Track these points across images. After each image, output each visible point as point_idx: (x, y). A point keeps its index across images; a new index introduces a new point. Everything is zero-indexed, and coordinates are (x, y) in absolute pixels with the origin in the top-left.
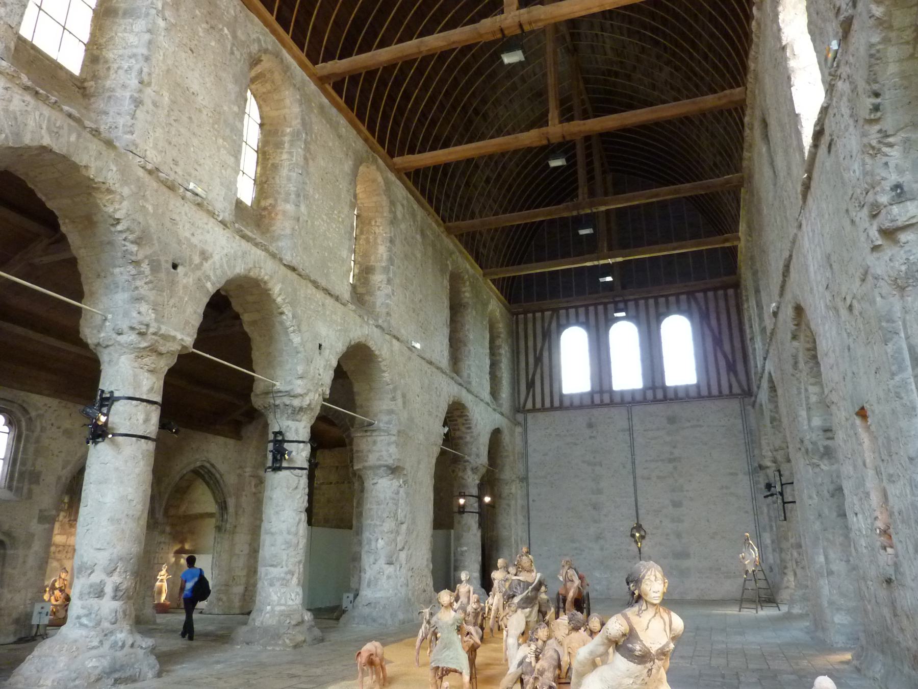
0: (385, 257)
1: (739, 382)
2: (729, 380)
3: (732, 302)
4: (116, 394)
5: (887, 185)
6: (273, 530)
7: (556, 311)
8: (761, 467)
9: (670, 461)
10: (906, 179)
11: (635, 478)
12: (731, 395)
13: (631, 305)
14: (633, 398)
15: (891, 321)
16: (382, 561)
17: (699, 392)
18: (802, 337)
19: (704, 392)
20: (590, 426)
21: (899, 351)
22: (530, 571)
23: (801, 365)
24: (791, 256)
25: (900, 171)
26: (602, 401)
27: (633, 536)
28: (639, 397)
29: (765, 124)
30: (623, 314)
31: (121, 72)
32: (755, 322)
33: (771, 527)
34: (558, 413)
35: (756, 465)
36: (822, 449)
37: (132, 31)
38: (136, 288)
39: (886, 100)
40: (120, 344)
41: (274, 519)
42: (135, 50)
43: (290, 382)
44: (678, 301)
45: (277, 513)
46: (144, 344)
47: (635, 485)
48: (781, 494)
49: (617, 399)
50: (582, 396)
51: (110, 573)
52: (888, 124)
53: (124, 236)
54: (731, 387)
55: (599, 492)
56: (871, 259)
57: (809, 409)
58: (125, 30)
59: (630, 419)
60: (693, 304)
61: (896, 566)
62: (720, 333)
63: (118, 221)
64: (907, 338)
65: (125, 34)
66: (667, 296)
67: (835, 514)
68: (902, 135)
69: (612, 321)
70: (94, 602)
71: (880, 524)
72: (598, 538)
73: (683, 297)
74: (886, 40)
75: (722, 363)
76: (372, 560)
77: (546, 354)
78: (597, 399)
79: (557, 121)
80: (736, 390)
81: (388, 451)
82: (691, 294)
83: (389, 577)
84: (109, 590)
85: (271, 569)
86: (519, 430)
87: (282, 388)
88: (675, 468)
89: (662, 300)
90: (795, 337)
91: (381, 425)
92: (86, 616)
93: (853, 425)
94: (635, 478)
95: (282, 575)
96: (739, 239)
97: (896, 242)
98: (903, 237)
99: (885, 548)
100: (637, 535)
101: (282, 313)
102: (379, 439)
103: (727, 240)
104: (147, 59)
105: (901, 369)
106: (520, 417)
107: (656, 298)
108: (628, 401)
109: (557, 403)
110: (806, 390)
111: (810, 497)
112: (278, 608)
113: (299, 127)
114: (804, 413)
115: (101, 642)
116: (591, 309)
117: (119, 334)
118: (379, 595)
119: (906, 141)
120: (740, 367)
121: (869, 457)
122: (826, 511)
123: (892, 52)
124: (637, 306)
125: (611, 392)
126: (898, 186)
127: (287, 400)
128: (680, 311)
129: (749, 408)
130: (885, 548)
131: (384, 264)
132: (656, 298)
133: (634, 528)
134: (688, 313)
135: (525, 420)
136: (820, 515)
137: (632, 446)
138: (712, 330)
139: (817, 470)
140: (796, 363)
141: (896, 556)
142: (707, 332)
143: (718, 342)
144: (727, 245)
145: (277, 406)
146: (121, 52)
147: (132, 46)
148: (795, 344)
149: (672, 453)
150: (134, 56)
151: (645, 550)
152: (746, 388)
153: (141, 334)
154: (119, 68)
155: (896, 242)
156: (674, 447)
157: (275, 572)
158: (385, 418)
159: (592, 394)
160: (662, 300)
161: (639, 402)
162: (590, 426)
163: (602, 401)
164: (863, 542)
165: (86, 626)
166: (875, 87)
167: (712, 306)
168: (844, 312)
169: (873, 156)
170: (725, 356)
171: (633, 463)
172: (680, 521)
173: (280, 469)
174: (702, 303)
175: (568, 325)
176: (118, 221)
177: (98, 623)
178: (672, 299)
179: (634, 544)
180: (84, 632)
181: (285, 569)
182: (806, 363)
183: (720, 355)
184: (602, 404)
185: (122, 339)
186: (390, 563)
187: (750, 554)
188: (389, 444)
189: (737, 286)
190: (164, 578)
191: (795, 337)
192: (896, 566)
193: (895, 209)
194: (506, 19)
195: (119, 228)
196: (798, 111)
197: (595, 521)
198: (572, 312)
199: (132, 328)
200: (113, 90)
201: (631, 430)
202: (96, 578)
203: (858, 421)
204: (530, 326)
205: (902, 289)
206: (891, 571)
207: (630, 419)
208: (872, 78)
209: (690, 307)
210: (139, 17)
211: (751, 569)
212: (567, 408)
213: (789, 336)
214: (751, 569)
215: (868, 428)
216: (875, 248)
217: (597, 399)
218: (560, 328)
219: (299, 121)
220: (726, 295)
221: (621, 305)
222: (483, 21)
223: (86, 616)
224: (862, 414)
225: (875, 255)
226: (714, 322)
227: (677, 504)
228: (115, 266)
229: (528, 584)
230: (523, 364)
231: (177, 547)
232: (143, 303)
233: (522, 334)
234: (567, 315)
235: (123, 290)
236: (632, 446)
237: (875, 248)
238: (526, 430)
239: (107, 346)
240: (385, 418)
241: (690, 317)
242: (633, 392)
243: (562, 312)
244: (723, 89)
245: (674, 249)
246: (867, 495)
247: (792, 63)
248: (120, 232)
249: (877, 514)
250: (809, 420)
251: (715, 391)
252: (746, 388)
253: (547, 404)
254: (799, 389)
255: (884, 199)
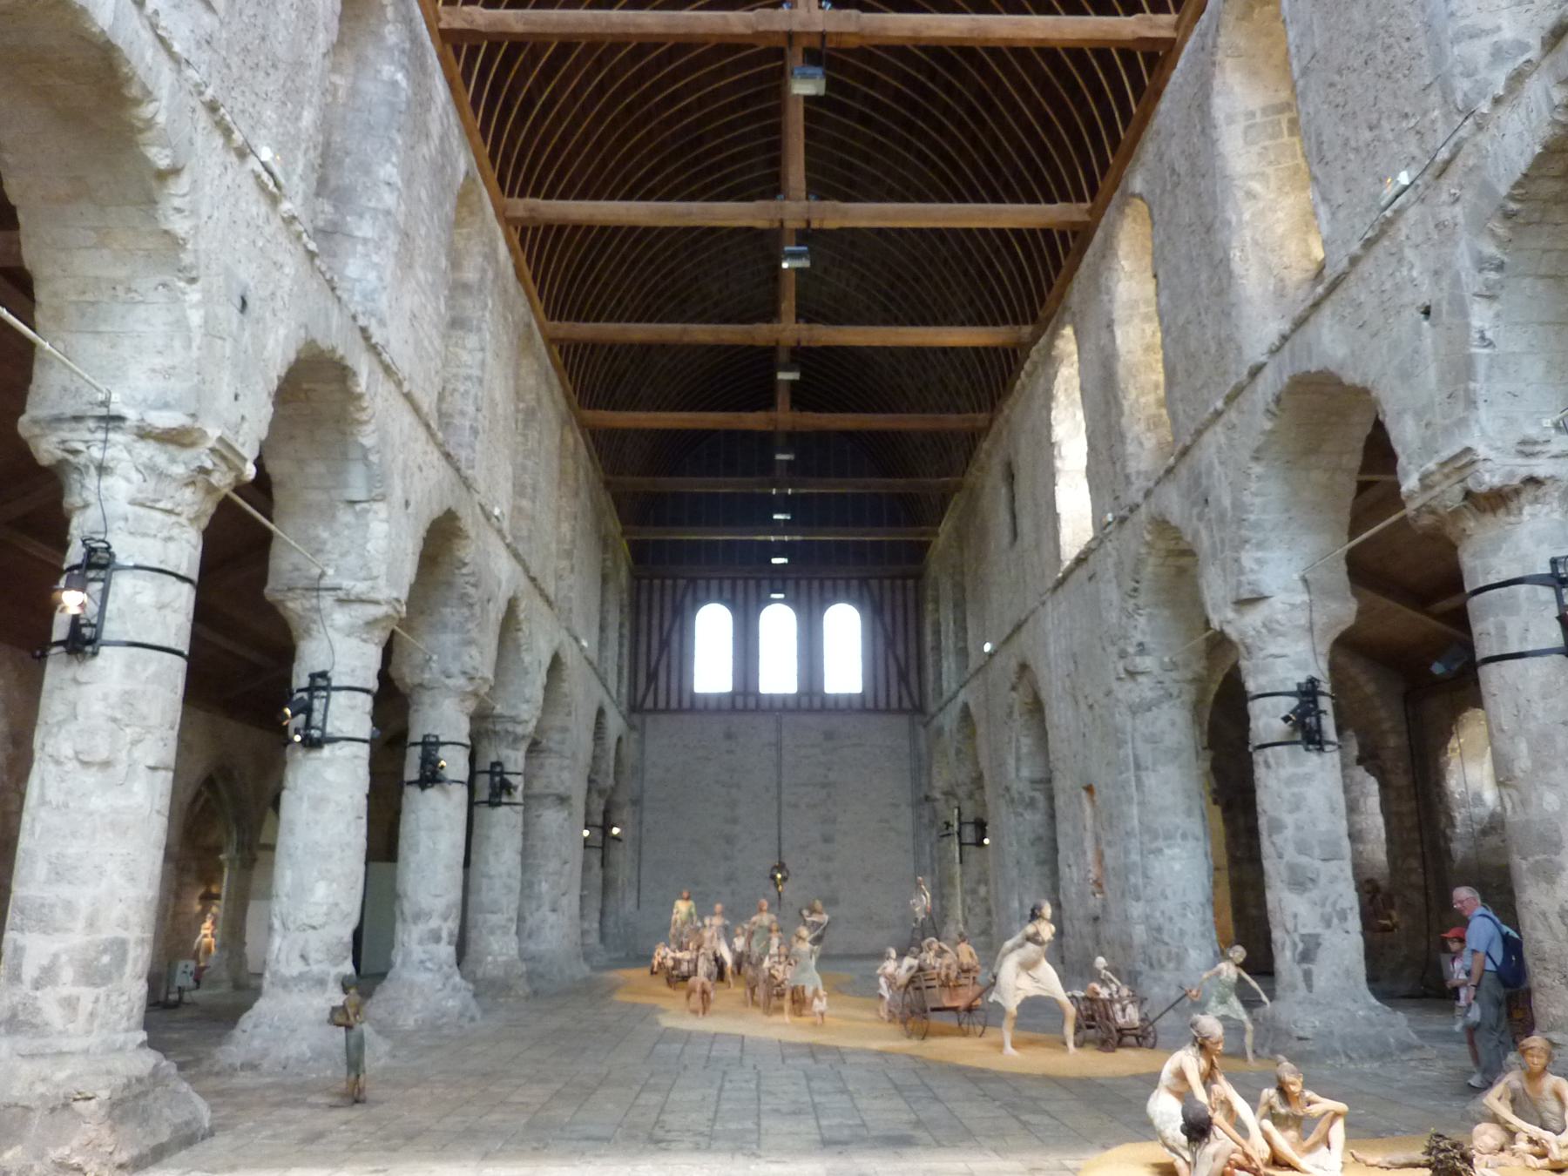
0: (568, 537)
1: (910, 694)
2: (899, 692)
3: (911, 595)
4: (442, 739)
5: (1135, 641)
6: (492, 873)
7: (692, 581)
8: (927, 798)
9: (824, 786)
10: (1147, 639)
11: (780, 805)
12: (901, 710)
13: (791, 584)
14: (784, 705)
15: (1124, 733)
16: (546, 908)
17: (863, 704)
18: (1021, 689)
19: (870, 705)
20: (729, 736)
21: (1127, 756)
22: (820, 913)
23: (1016, 715)
24: (1026, 620)
25: (1144, 633)
26: (745, 705)
27: (773, 877)
28: (791, 704)
29: (1010, 477)
30: (781, 596)
31: (457, 395)
32: (947, 637)
33: (933, 870)
34: (687, 717)
35: (922, 795)
36: (1027, 800)
37: (464, 347)
38: (469, 631)
39: (1143, 586)
40: (447, 687)
41: (492, 859)
42: (470, 371)
43: (514, 707)
44: (848, 587)
45: (496, 854)
46: (470, 689)
47: (779, 812)
48: (959, 834)
49: (764, 704)
50: (720, 697)
51: (445, 919)
52: (1141, 600)
53: (467, 579)
54: (900, 699)
55: (735, 821)
56: (1115, 685)
57: (1018, 759)
58: (456, 345)
59: (779, 731)
60: (866, 594)
61: (1104, 907)
62: (894, 632)
63: (465, 564)
64: (1134, 748)
65: (457, 350)
66: (835, 579)
67: (1033, 862)
68: (1148, 610)
69: (765, 601)
70: (432, 947)
71: (1092, 876)
72: (730, 878)
73: (854, 583)
74: (1149, 554)
75: (893, 670)
76: (534, 906)
77: (675, 637)
78: (739, 703)
79: (788, 406)
80: (906, 704)
81: (559, 777)
82: (864, 581)
83: (552, 927)
84: (445, 934)
85: (489, 916)
86: (635, 735)
87: (507, 713)
88: (829, 795)
89: (828, 583)
90: (1014, 688)
91: (551, 745)
92: (430, 960)
93: (1078, 796)
94: (780, 805)
95: (503, 923)
96: (936, 534)
97: (1135, 680)
98: (1141, 679)
99: (1094, 894)
100: (779, 876)
101: (519, 630)
102: (550, 761)
103: (923, 534)
104: (481, 381)
105: (1128, 770)
106: (636, 719)
107: (822, 580)
108: (778, 708)
109: (686, 704)
110: (1018, 740)
111: (1011, 845)
112: (501, 959)
113: (533, 403)
114: (1011, 762)
115: (444, 985)
116: (740, 583)
117: (448, 677)
118: (543, 947)
119: (1151, 614)
120: (913, 677)
121: (1089, 822)
122: (1025, 859)
123: (1151, 560)
124: (797, 584)
125: (757, 695)
126: (1141, 644)
127: (510, 727)
128: (848, 600)
129: (921, 730)
130: (1094, 894)
131: (566, 547)
132: (822, 580)
133: (775, 867)
134: (859, 603)
135: (643, 723)
136: (1018, 862)
137: (779, 766)
138: (883, 625)
139: (1020, 819)
140: (1010, 714)
141: (1105, 899)
142: (879, 626)
143: (890, 643)
144: (923, 539)
145: (495, 733)
146: (455, 370)
147: (466, 366)
148: (1014, 694)
149: (826, 776)
150: (468, 378)
151: (786, 895)
152: (917, 703)
153: (472, 679)
154: (454, 390)
155: (1135, 680)
156: (829, 769)
157: (494, 919)
158: (557, 737)
159: (733, 695)
160: (828, 583)
161: (792, 711)
162: (729, 736)
163: (745, 705)
164: (1073, 890)
165: (430, 970)
166: (1137, 577)
167: (888, 596)
168: (1083, 708)
169: (1128, 618)
170: (897, 659)
171: (779, 785)
172: (829, 859)
173: (500, 804)
174: (876, 592)
175: (708, 600)
176: (465, 564)
177: (440, 968)
178: (841, 583)
179: (773, 888)
180: (429, 976)
181: (506, 916)
182: (1021, 715)
183: (891, 661)
184: (745, 710)
185: (449, 682)
186: (554, 910)
187: (921, 900)
188: (561, 768)
189: (919, 577)
190: (208, 932)
191: (1014, 688)
192: (1104, 907)
193: (1138, 660)
194: (784, 330)
195: (464, 571)
196: (1058, 511)
197: (727, 858)
198: (714, 584)
199: (464, 673)
200: (451, 416)
201: (778, 746)
202: (434, 923)
203: (1084, 794)
204: (656, 597)
205: (1134, 713)
206: (1099, 911)
207: (779, 731)
208: (1136, 570)
209: (861, 595)
210: (471, 331)
211: (921, 916)
212: (699, 711)
213: (1008, 685)
214: (921, 916)
215: (1093, 802)
216: (1119, 679)
217: (739, 703)
218: (697, 603)
219: (533, 396)
220: (904, 587)
221: (778, 584)
222: (757, 325)
223: (430, 960)
224: (1089, 789)
225: (1119, 683)
226: (888, 618)
227: (827, 840)
228: (445, 605)
229: (819, 925)
230: (643, 648)
231: (201, 891)
232: (474, 647)
233: (644, 606)
234: (708, 589)
235: (453, 631)
236: (779, 766)
237: (1119, 679)
238: (643, 735)
239: (432, 688)
240: (557, 737)
241: (861, 609)
242: (785, 697)
243: (702, 583)
244: (967, 412)
245: (868, 534)
246: (1085, 853)
247: (1058, 463)
248: (464, 575)
249: (1091, 868)
250: (1018, 770)
251: (882, 705)
252: (917, 703)
253: (674, 704)
254: (1010, 738)
255: (1131, 650)
